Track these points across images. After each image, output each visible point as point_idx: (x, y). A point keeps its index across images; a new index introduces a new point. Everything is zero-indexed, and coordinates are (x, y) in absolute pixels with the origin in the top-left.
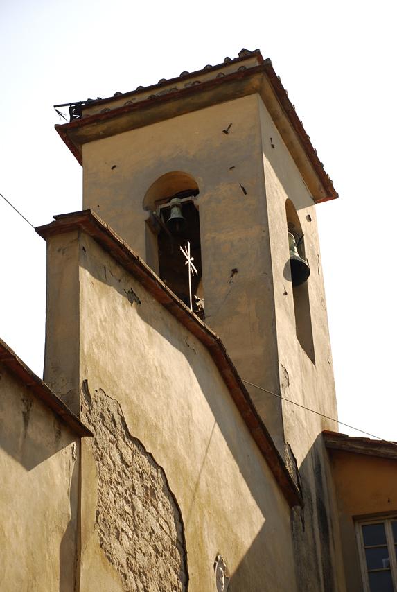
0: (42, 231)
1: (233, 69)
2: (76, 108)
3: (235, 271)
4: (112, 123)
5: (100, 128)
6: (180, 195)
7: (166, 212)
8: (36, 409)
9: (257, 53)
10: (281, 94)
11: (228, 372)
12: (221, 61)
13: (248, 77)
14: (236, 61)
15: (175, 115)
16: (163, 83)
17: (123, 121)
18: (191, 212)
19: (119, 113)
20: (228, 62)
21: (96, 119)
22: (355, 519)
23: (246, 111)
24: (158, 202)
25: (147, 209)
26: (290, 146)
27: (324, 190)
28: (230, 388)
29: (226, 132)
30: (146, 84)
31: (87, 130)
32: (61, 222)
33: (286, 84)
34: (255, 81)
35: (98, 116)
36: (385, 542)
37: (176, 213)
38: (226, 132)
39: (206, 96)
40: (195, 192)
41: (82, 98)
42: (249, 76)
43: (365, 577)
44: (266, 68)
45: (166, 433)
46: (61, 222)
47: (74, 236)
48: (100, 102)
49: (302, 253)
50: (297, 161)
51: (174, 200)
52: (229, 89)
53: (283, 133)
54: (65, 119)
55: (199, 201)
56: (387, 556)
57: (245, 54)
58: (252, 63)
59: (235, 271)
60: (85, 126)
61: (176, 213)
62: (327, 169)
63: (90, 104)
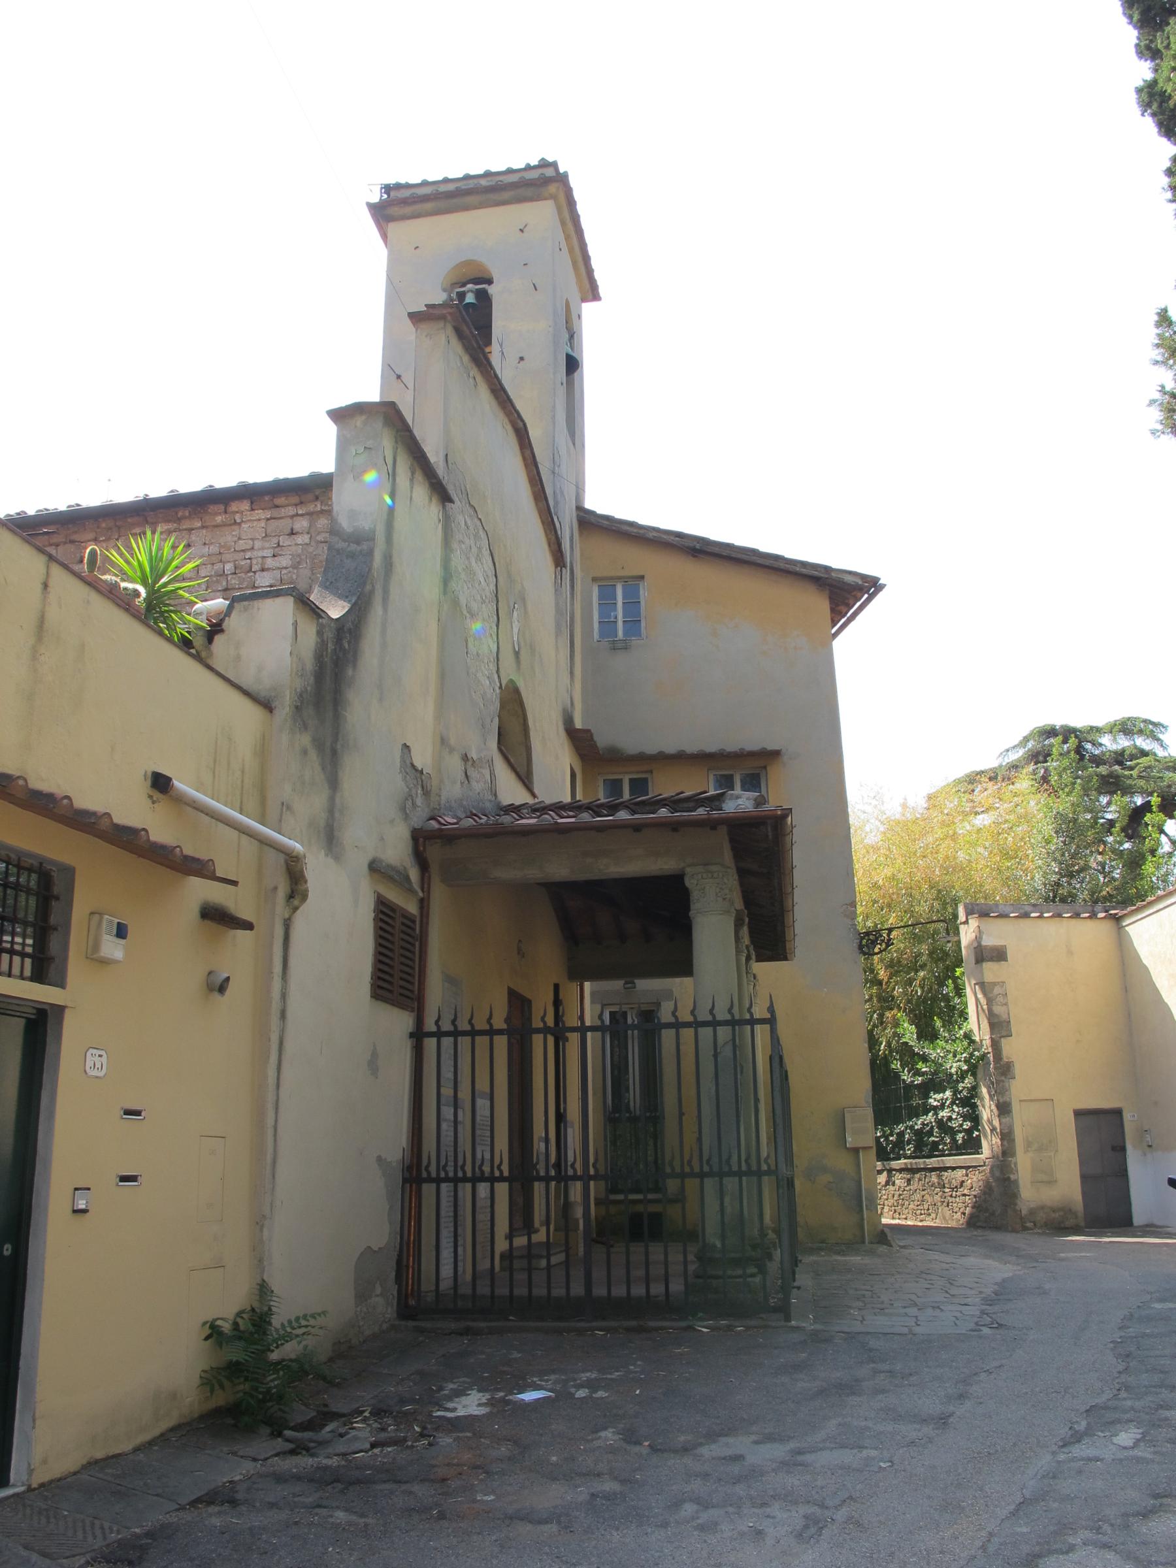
0: (411, 316)
1: (534, 175)
2: (387, 189)
3: (522, 359)
4: (418, 207)
5: (408, 210)
6: (477, 281)
7: (462, 296)
8: (419, 476)
9: (554, 165)
10: (571, 203)
11: (528, 452)
12: (523, 166)
13: (542, 184)
14: (535, 167)
15: (476, 208)
16: (467, 177)
17: (429, 206)
18: (484, 299)
19: (425, 199)
20: (528, 168)
21: (404, 202)
22: (594, 580)
23: (539, 215)
24: (454, 285)
25: (444, 290)
26: (571, 250)
27: (591, 292)
28: (526, 466)
29: (521, 230)
30: (515, 167)
31: (395, 211)
32: (431, 311)
33: (577, 195)
34: (552, 188)
35: (406, 198)
36: (615, 599)
37: (470, 298)
38: (521, 230)
39: (506, 195)
40: (490, 282)
41: (392, 181)
42: (544, 184)
43: (596, 626)
44: (562, 180)
45: (1030, 745)
46: (431, 311)
47: (441, 324)
48: (408, 186)
49: (572, 348)
50: (574, 264)
51: (470, 286)
52: (529, 192)
53: (567, 238)
54: (375, 198)
55: (492, 290)
56: (615, 610)
57: (544, 164)
58: (549, 172)
59: (522, 359)
60: (397, 206)
61: (470, 298)
62: (597, 275)
63: (398, 186)
